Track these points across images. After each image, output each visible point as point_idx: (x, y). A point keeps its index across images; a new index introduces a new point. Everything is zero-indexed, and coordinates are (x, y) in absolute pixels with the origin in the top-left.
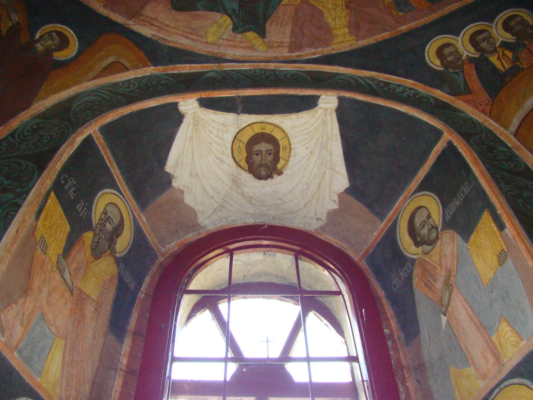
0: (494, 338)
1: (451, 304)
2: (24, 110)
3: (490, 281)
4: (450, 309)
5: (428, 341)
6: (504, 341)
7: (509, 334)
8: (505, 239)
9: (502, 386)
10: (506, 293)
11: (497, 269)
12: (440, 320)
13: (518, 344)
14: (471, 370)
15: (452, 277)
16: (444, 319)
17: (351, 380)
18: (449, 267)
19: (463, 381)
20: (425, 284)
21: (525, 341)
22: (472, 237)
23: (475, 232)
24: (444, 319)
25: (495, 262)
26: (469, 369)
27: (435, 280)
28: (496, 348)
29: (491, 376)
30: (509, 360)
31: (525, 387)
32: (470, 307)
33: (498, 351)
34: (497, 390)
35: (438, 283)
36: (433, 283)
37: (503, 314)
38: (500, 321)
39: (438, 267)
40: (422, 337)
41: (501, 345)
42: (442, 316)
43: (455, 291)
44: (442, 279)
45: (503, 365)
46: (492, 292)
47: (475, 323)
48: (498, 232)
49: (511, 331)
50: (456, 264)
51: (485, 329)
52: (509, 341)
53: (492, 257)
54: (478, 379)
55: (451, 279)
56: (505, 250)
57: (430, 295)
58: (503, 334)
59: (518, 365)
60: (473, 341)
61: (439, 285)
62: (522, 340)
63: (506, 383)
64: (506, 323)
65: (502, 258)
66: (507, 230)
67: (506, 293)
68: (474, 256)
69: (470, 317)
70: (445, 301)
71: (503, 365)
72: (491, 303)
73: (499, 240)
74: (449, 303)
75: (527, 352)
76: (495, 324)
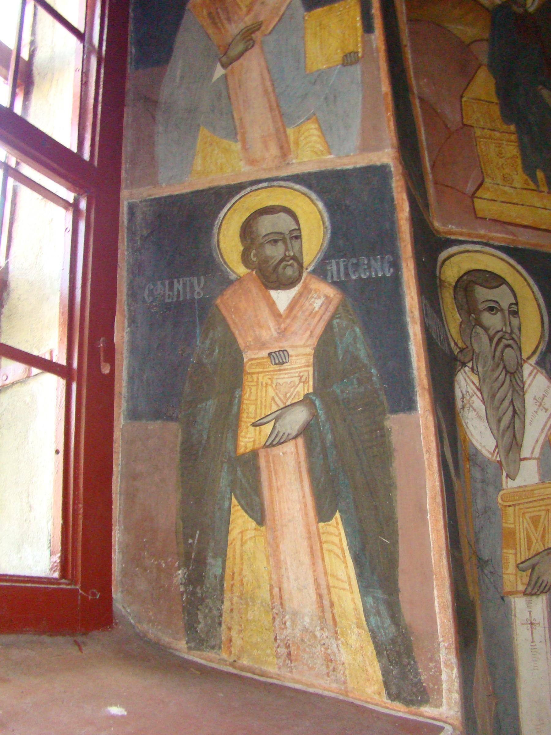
0: (290, 131)
1: (241, 60)
2: (111, 491)
3: (317, 71)
4: (236, 64)
5: (178, 80)
6: (304, 142)
7: (314, 138)
8: (366, 44)
9: (275, 183)
10: (335, 97)
11: (337, 65)
12: (211, 70)
13: (322, 154)
14: (237, 147)
15: (260, 31)
16: (219, 71)
17: (8, 106)
18: (262, 18)
19: (216, 152)
20: (210, 14)
21: (332, 156)
22: (319, 10)
23: (326, 8)
24: (219, 71)
25: (338, 57)
26: (233, 144)
27: (229, 20)
28: (288, 142)
29: (264, 166)
30: (300, 164)
31: (307, 199)
32: (272, 81)
33: (289, 146)
34: (265, 184)
35: (234, 26)
36: (225, 22)
37: (317, 114)
38: (308, 119)
39: (244, 9)
40: (168, 69)
41: (297, 143)
42: (219, 66)
43: (256, 50)
44: (242, 26)
45: (288, 164)
46: (315, 83)
47: (269, 101)
48: (360, 32)
49: (319, 137)
50: (274, 23)
51: (281, 115)
52: (310, 144)
53: (337, 50)
54: (241, 160)
55: (258, 33)
56: (360, 55)
57: (210, 31)
58: (306, 134)
59: (310, 174)
60: (257, 117)
61: (234, 29)
62: (330, 154)
63: (282, 183)
64: (317, 126)
65: (349, 59)
66: (373, 37)
67: (335, 97)
68: (309, 31)
69: (266, 91)
70: (233, 53)
71: (288, 164)
72: (307, 94)
73: (357, 40)
74: (238, 57)
75: (330, 168)
76: (299, 118)
